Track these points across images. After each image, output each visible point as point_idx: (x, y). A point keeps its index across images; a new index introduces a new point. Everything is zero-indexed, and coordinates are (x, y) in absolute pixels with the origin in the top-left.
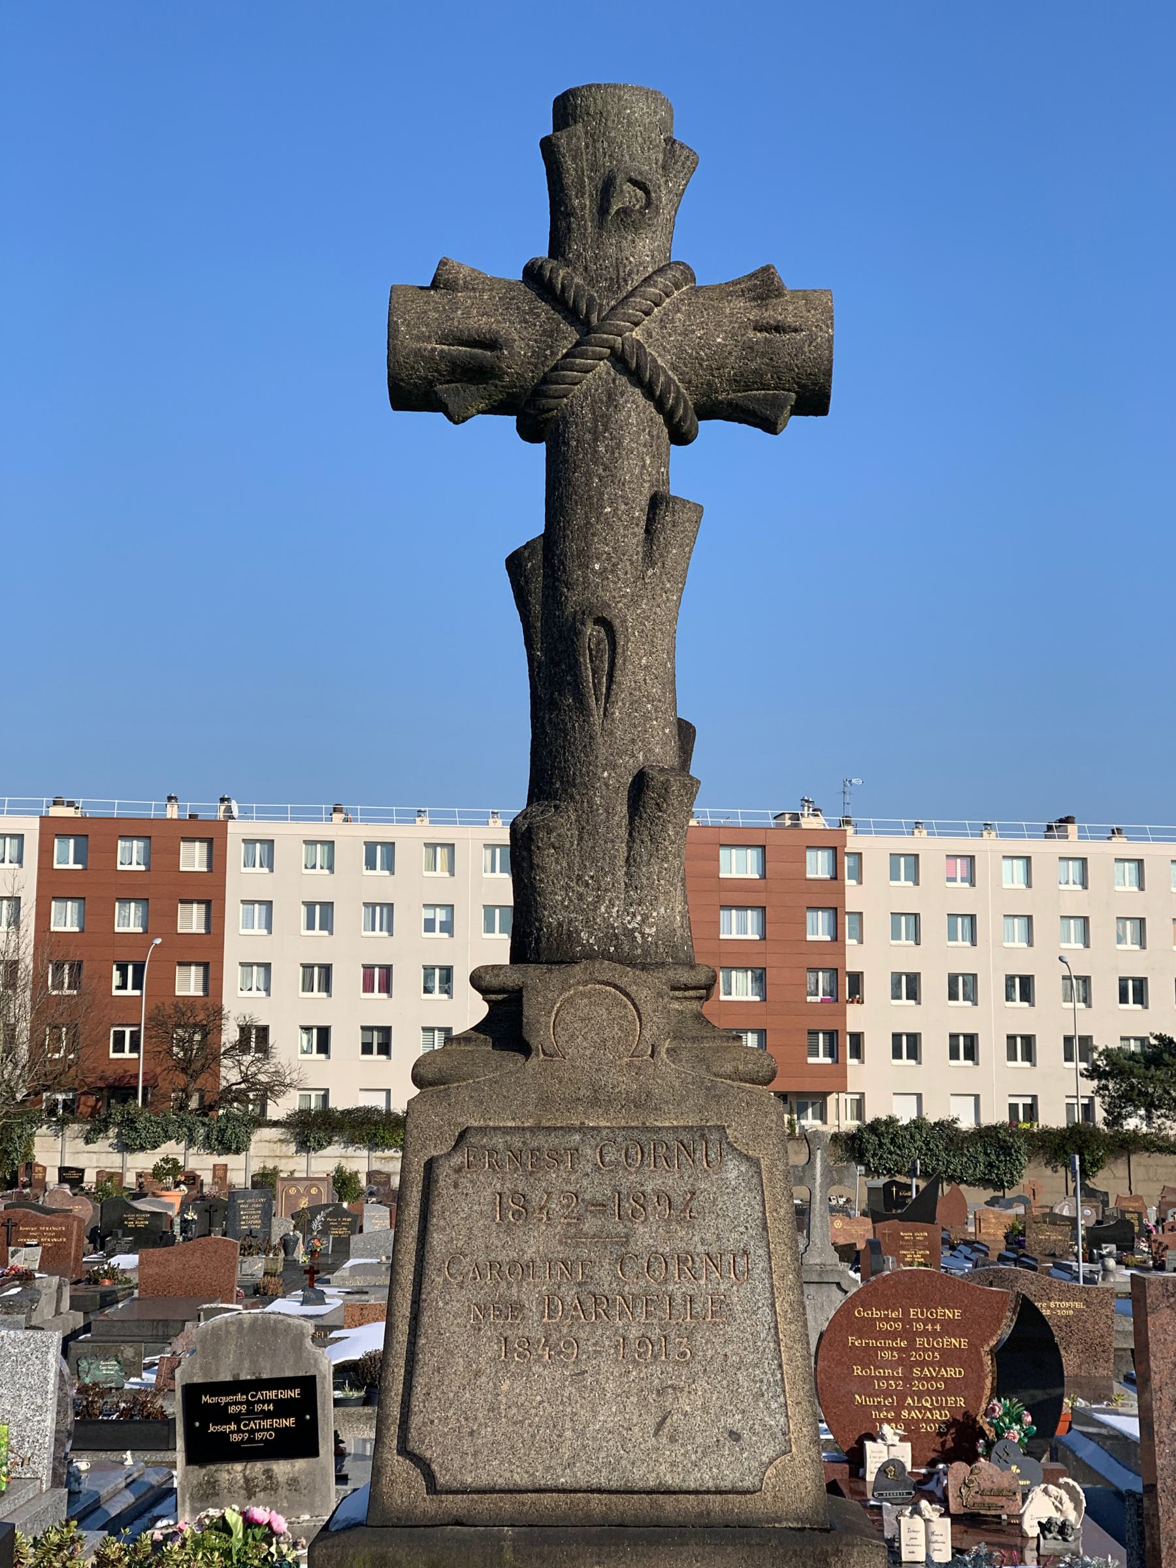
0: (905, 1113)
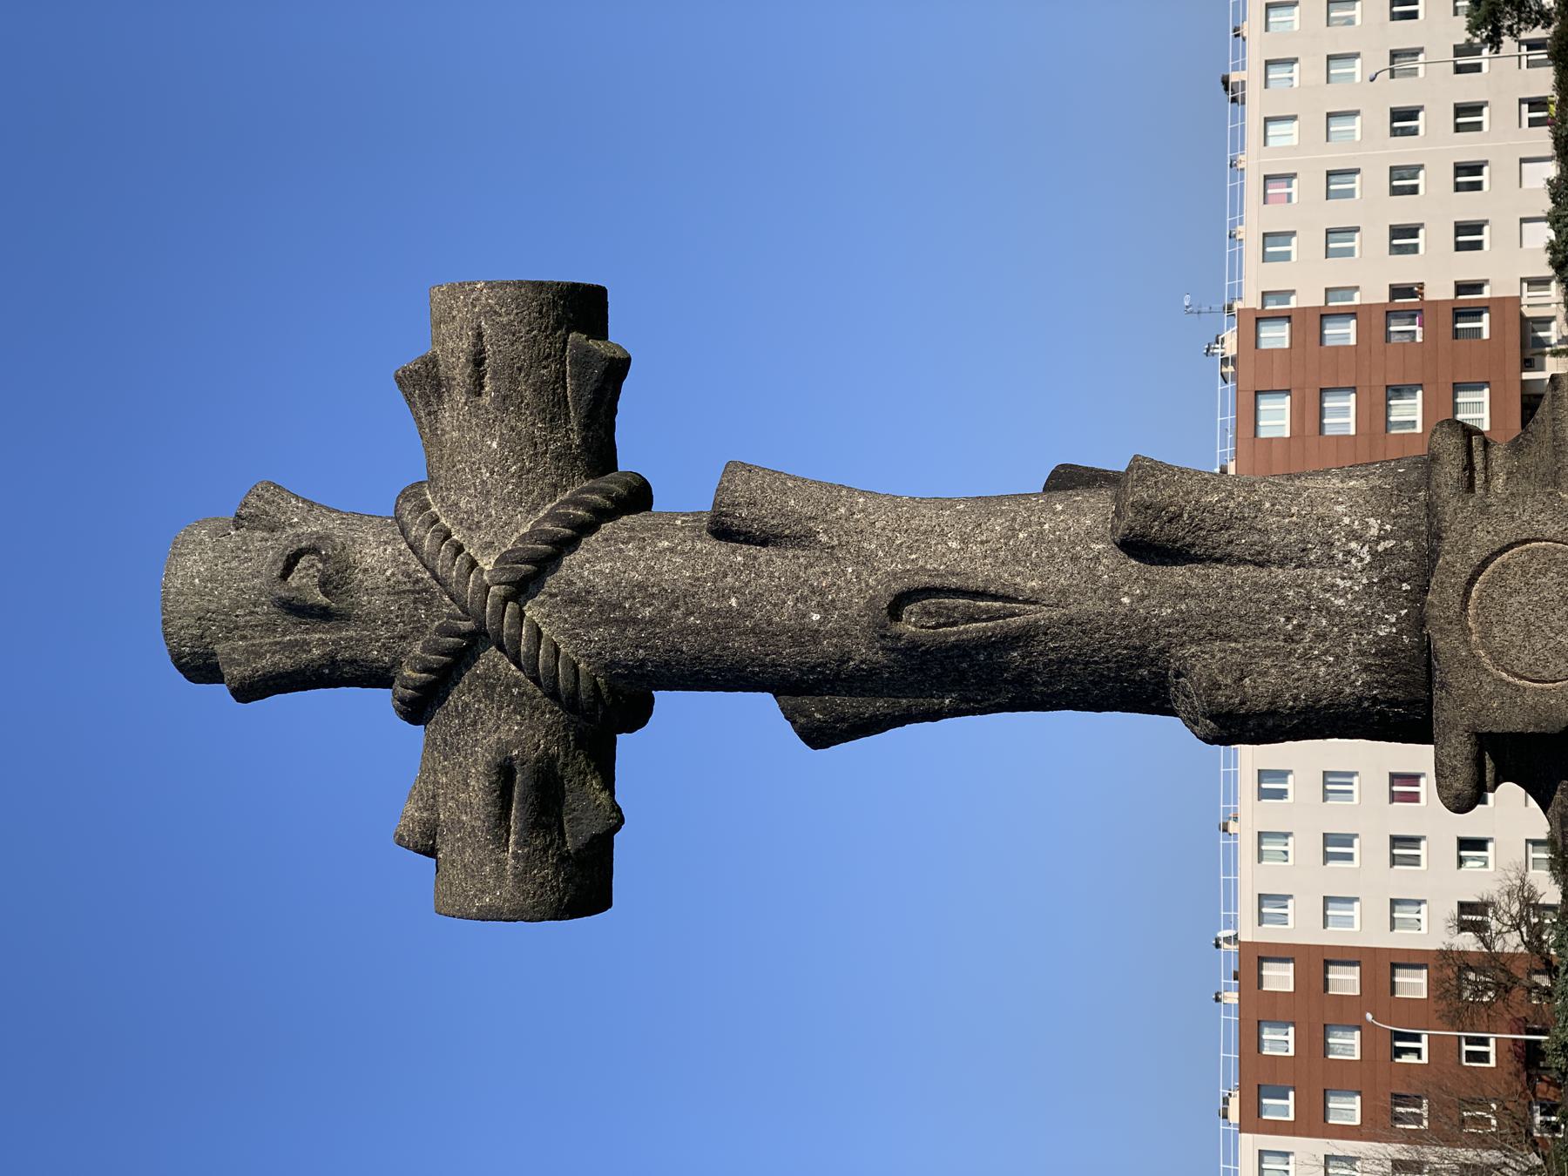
0: (1544, 234)
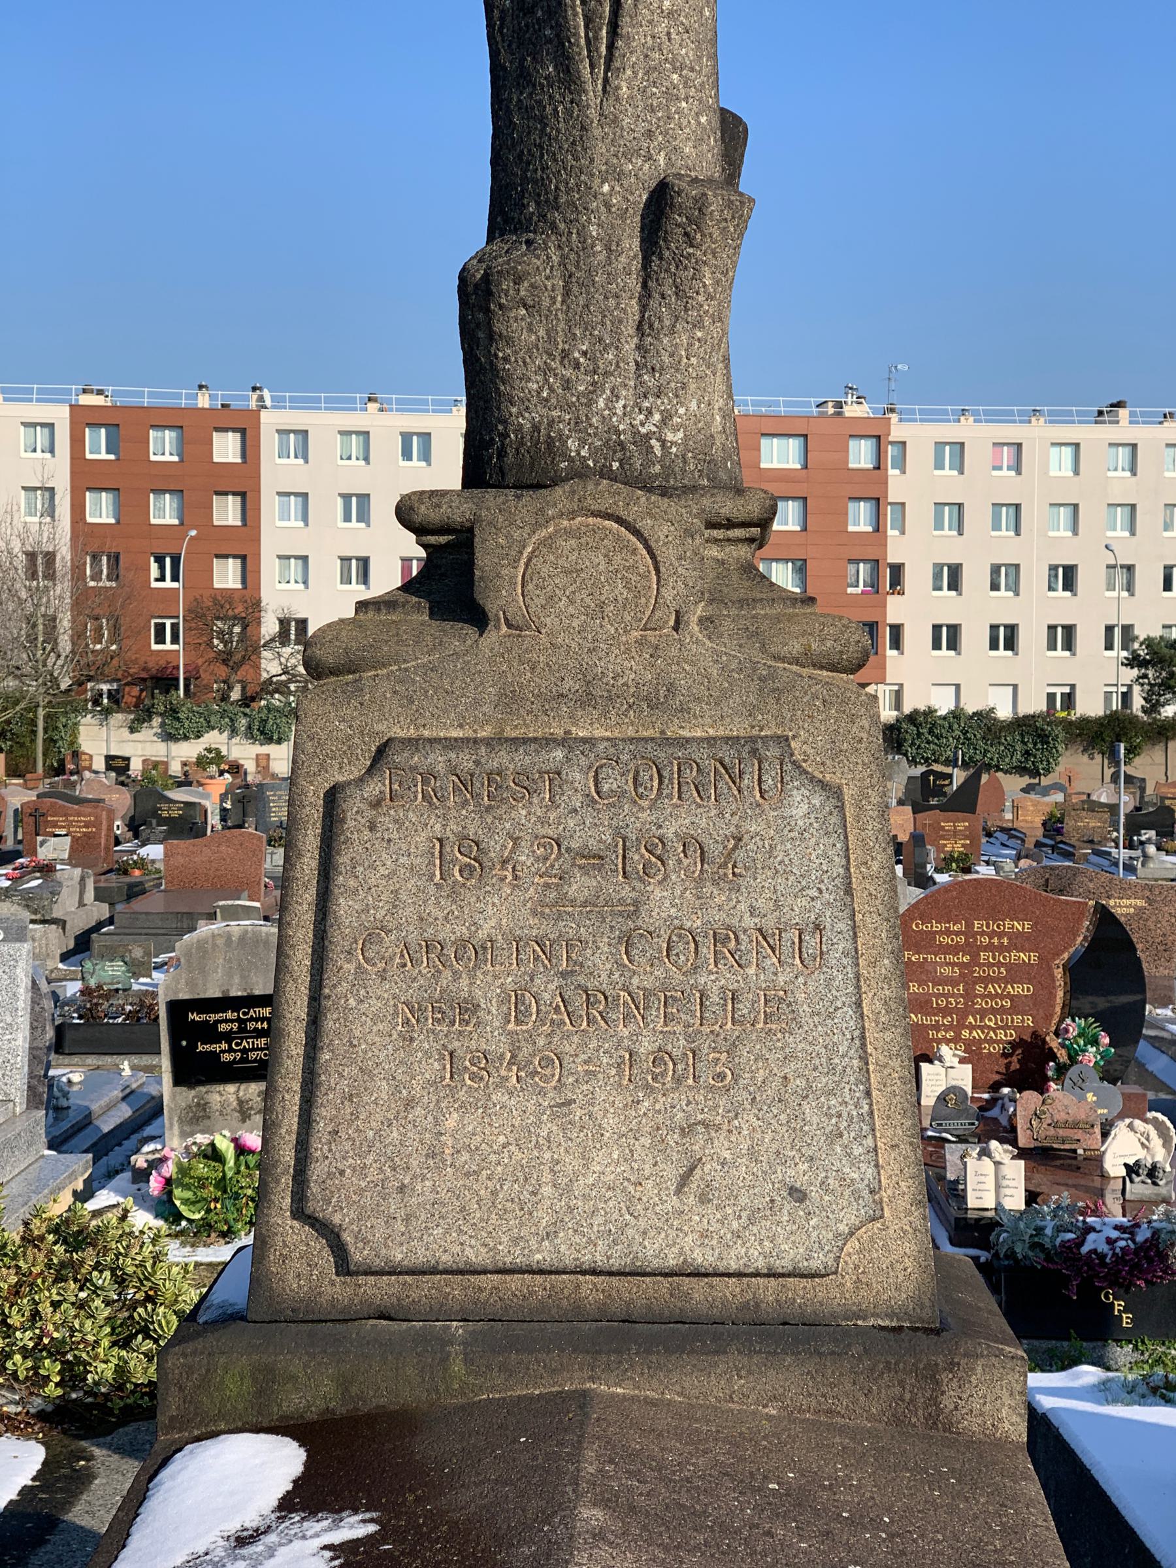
0: (943, 704)
